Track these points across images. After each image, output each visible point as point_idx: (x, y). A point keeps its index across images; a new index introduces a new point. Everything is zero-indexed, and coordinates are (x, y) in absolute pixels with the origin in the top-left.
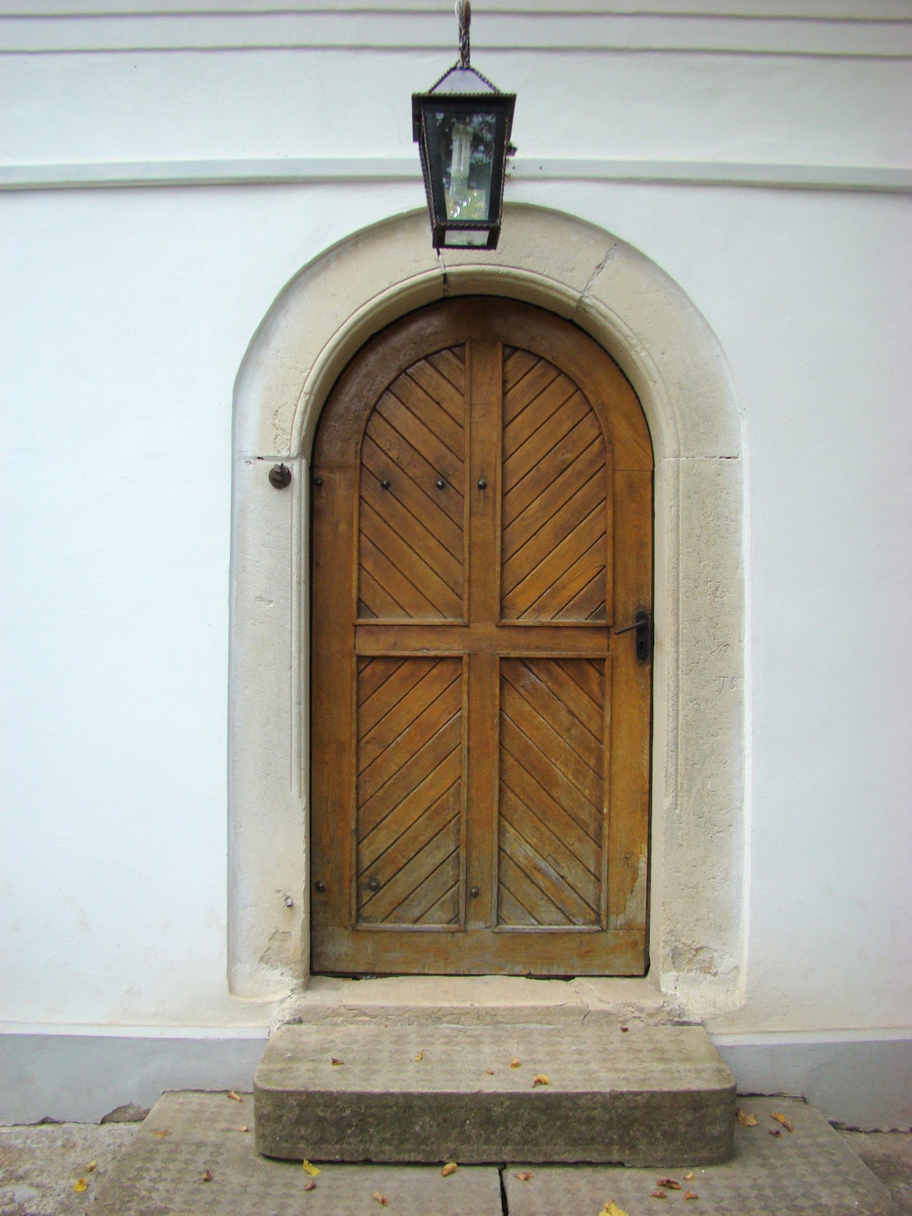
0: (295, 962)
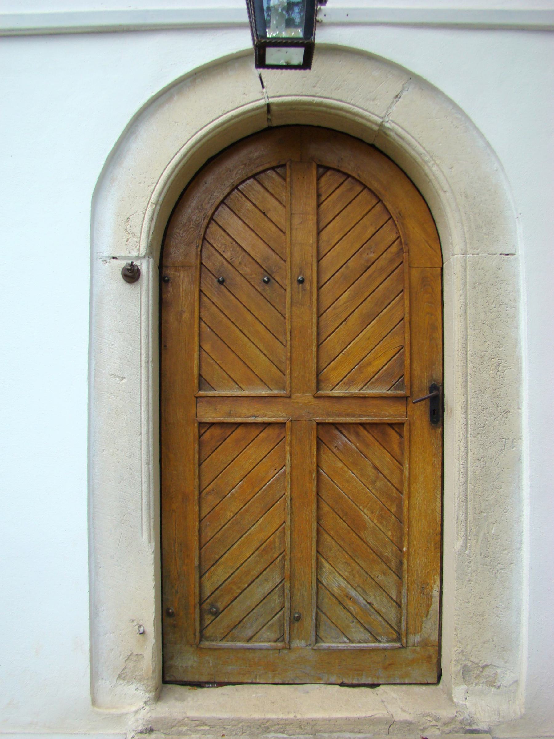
0: (147, 679)
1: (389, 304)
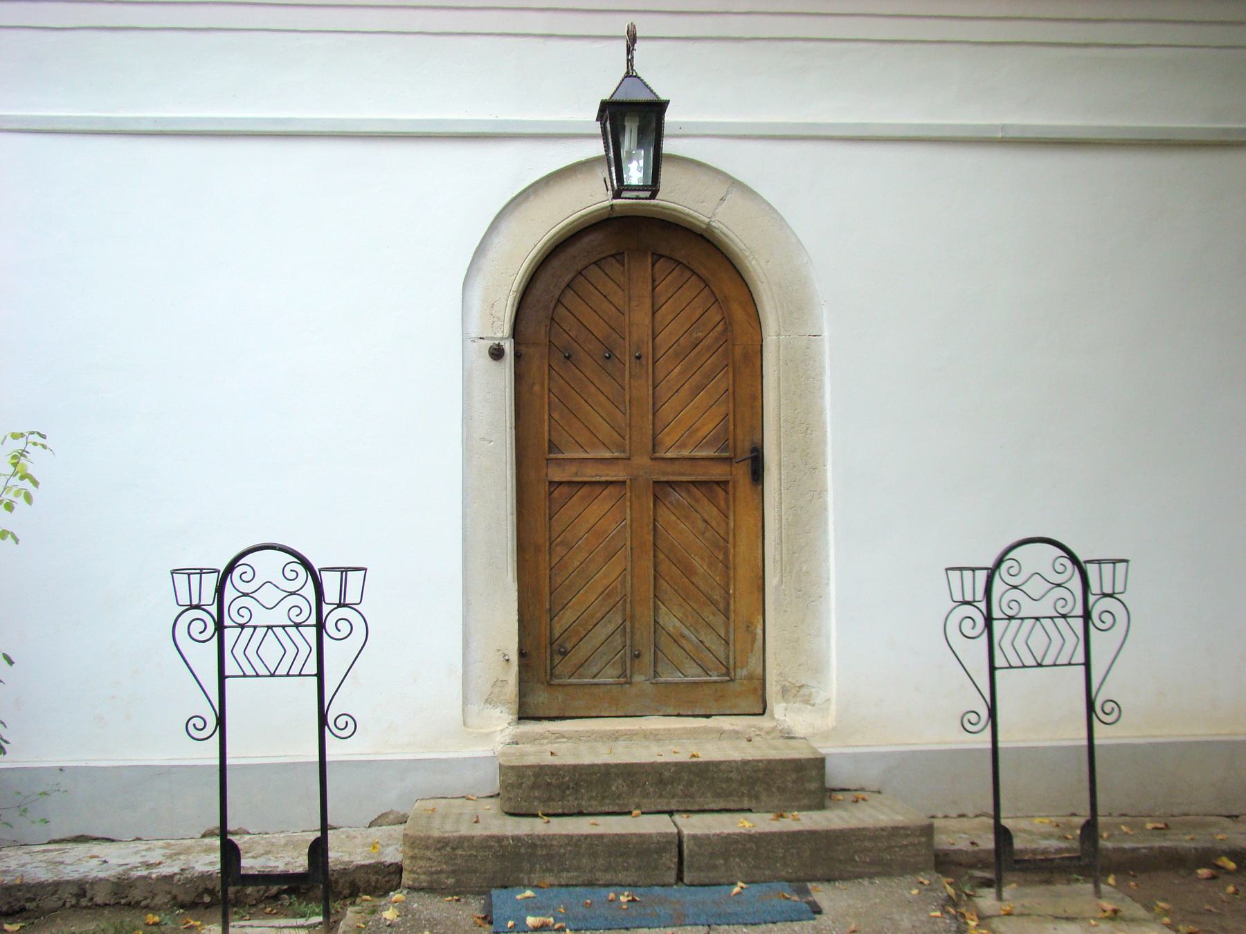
1: (716, 377)
